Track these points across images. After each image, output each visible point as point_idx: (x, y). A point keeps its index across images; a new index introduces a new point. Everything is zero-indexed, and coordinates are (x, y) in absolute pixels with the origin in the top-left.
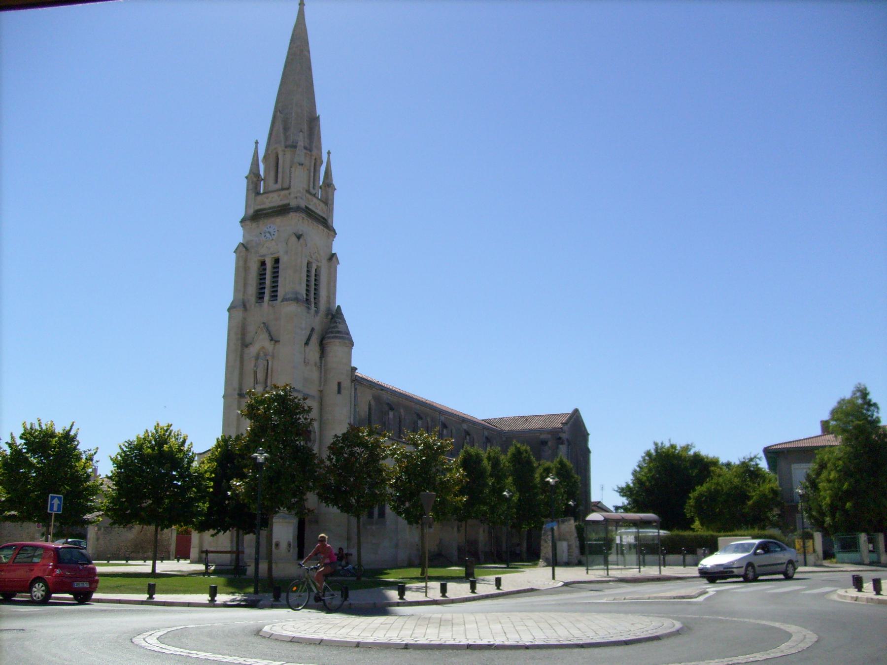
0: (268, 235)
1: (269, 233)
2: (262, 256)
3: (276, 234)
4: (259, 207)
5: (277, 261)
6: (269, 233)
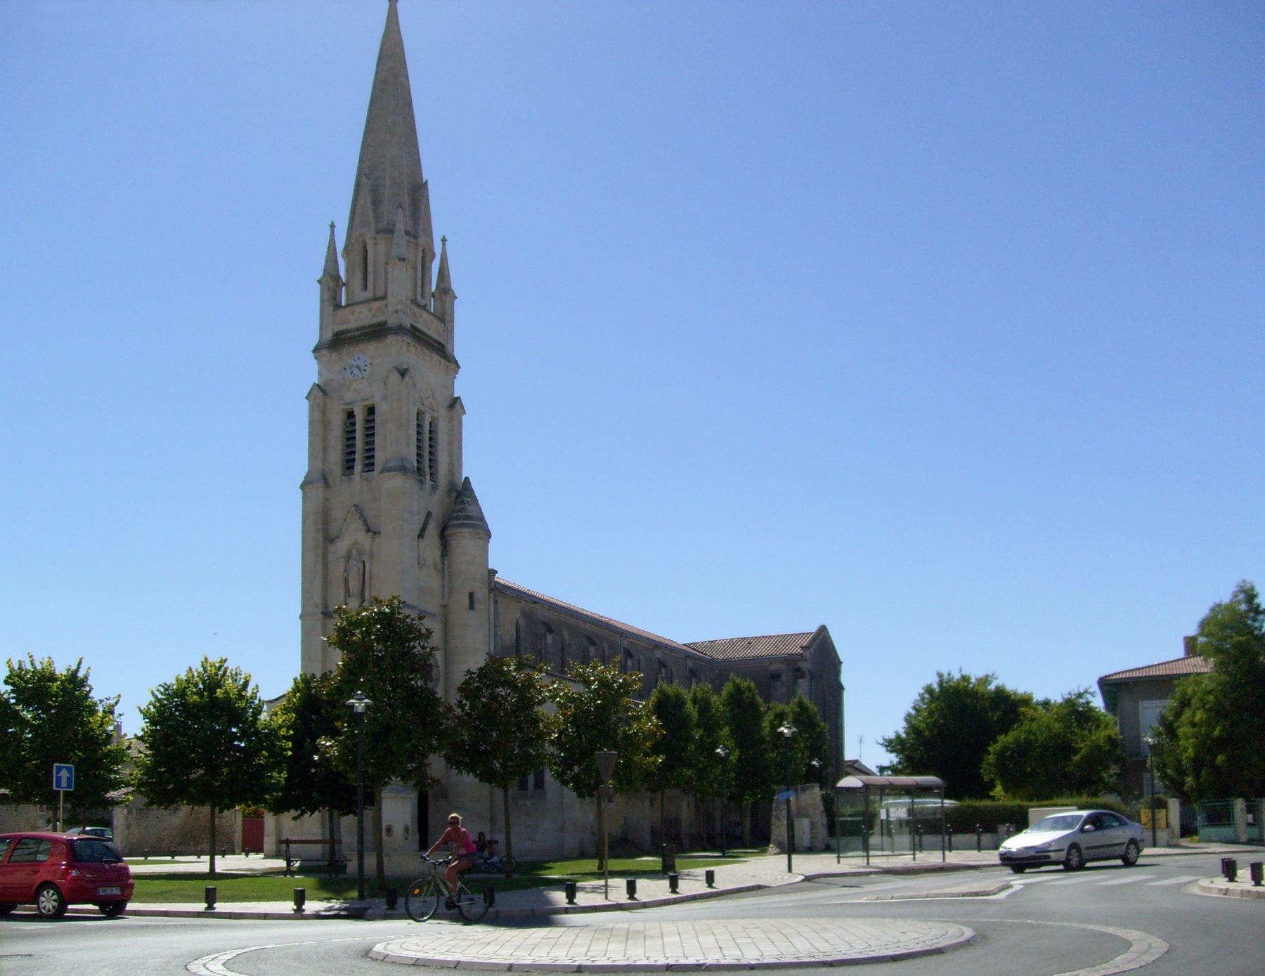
0: (356, 371)
1: (358, 367)
2: (348, 404)
3: (368, 369)
4: (345, 327)
5: (371, 410)
6: (358, 367)
